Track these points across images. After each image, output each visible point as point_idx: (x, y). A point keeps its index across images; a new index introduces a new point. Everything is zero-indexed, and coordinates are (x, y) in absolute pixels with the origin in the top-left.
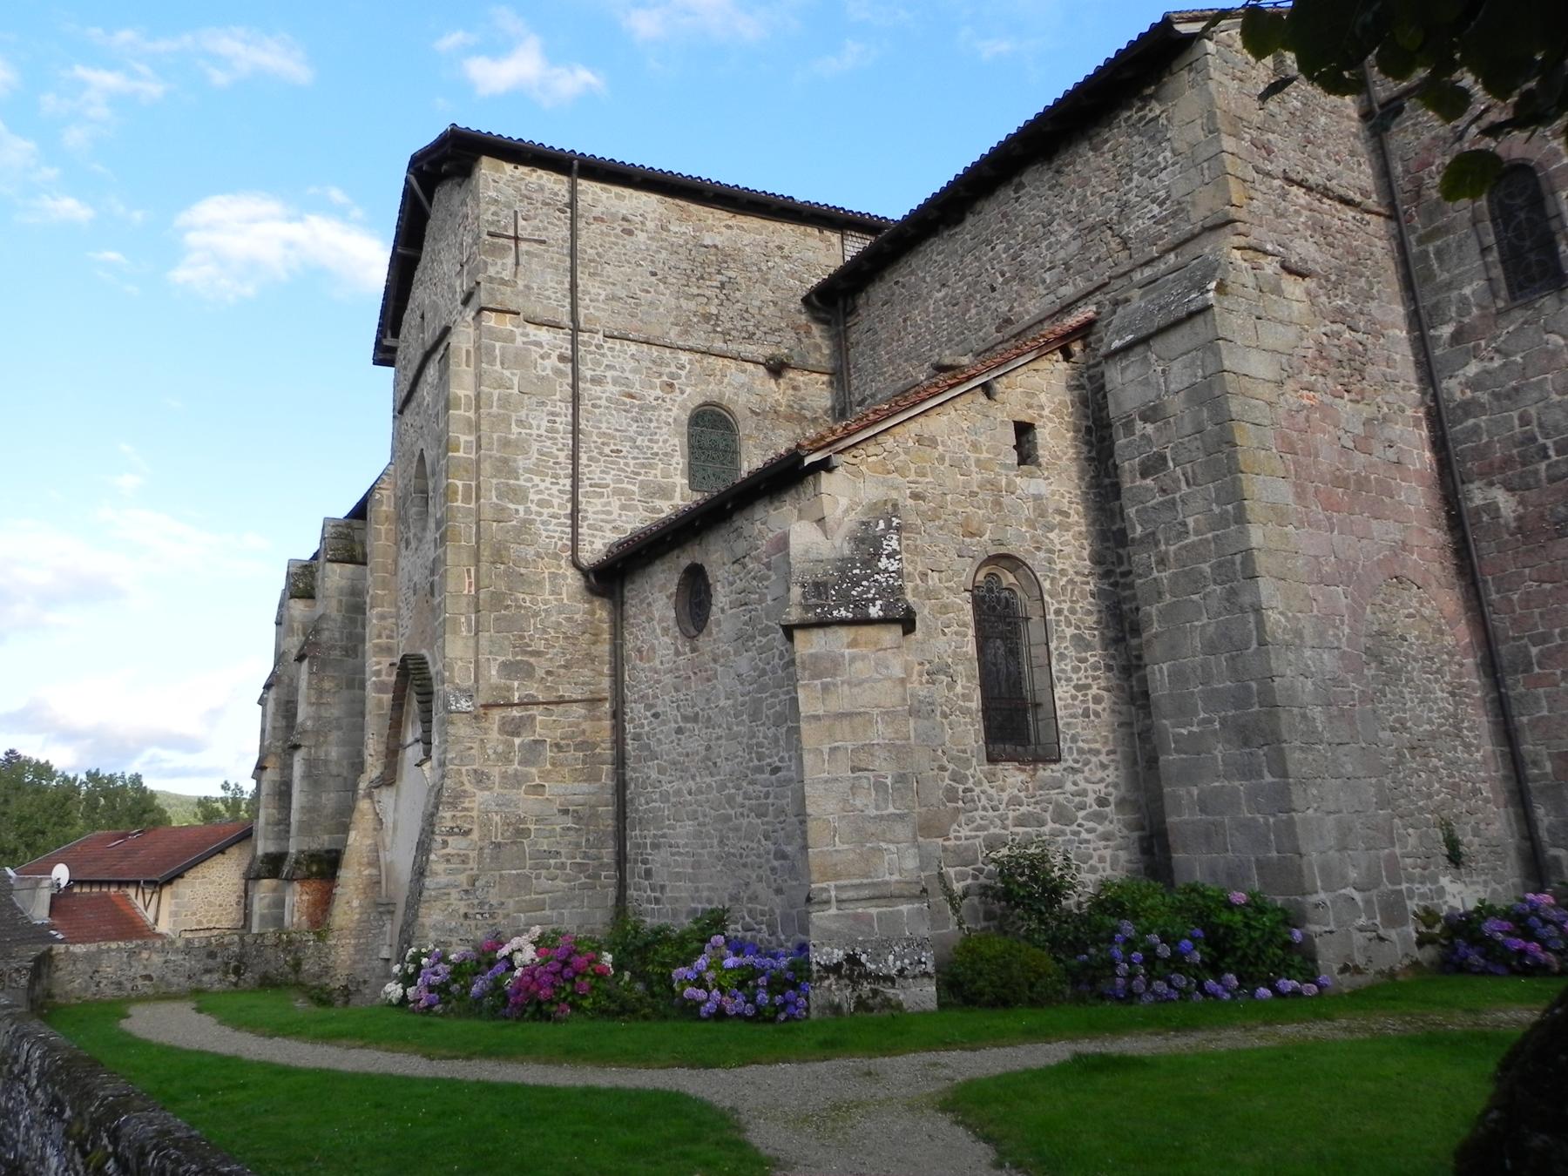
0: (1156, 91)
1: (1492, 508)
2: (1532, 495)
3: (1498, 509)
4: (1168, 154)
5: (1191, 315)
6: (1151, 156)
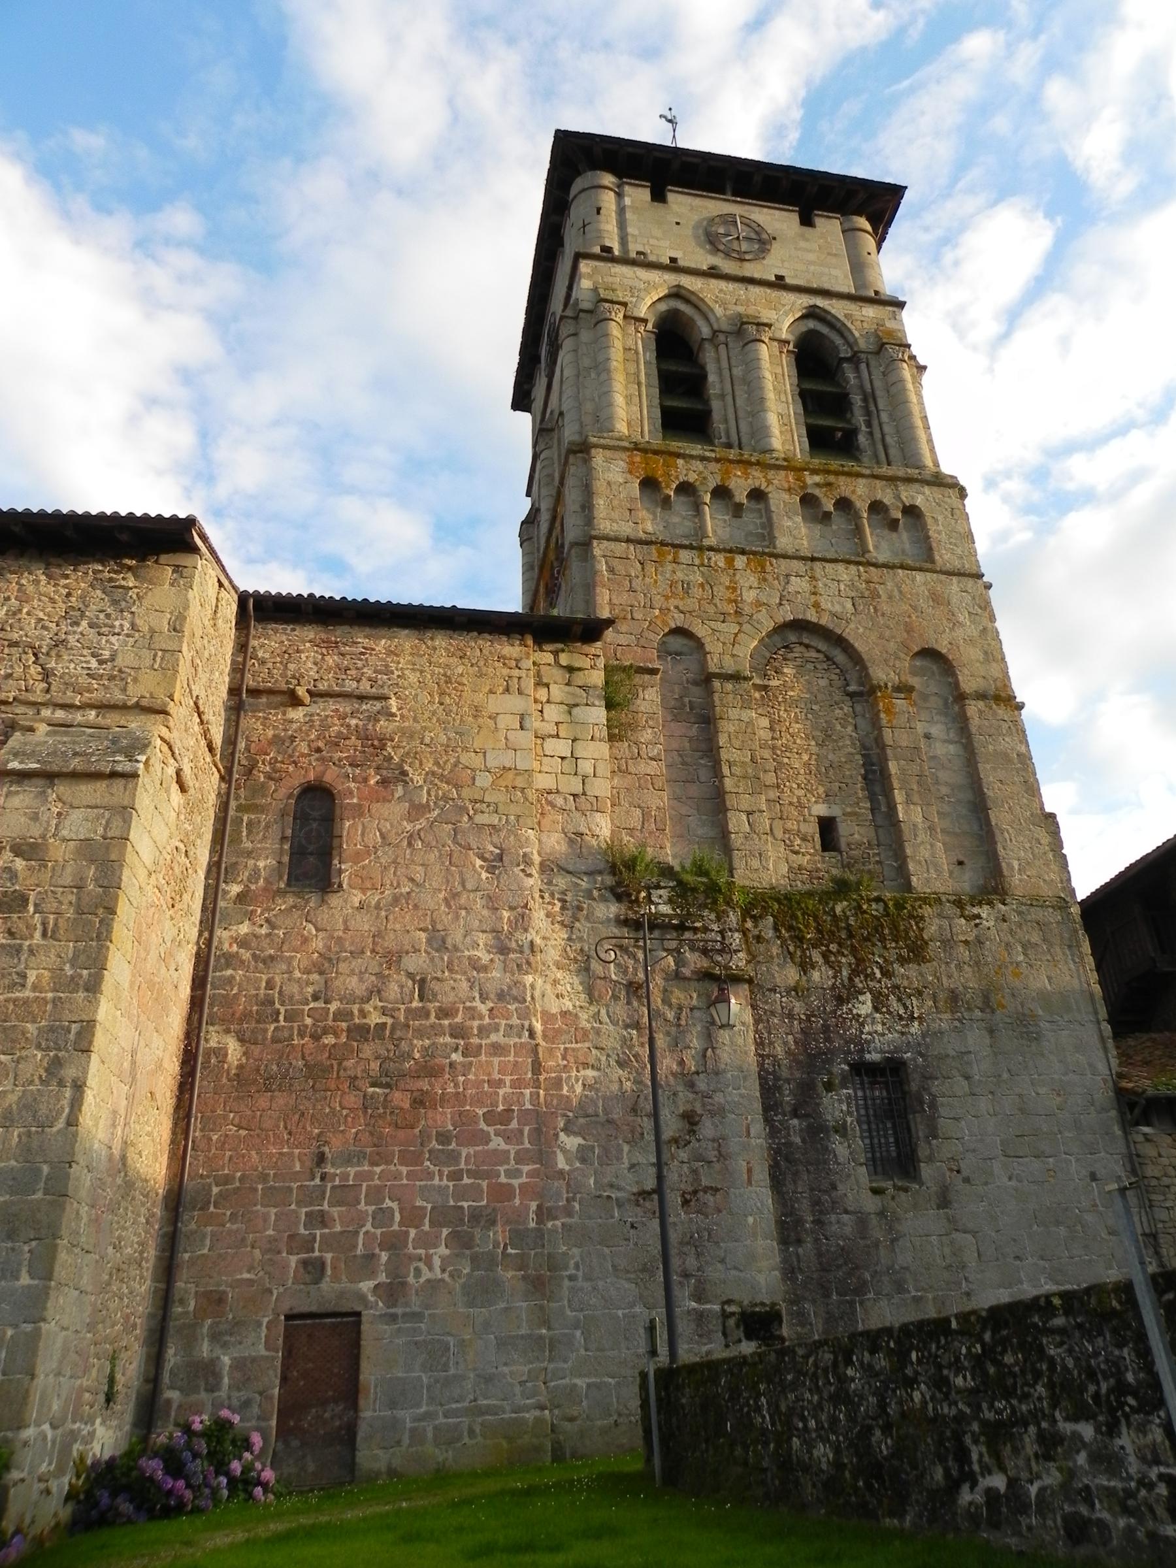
0: (137, 567)
1: (221, 1053)
2: (256, 1050)
3: (226, 1055)
4: (127, 625)
5: (114, 775)
6: (108, 616)
